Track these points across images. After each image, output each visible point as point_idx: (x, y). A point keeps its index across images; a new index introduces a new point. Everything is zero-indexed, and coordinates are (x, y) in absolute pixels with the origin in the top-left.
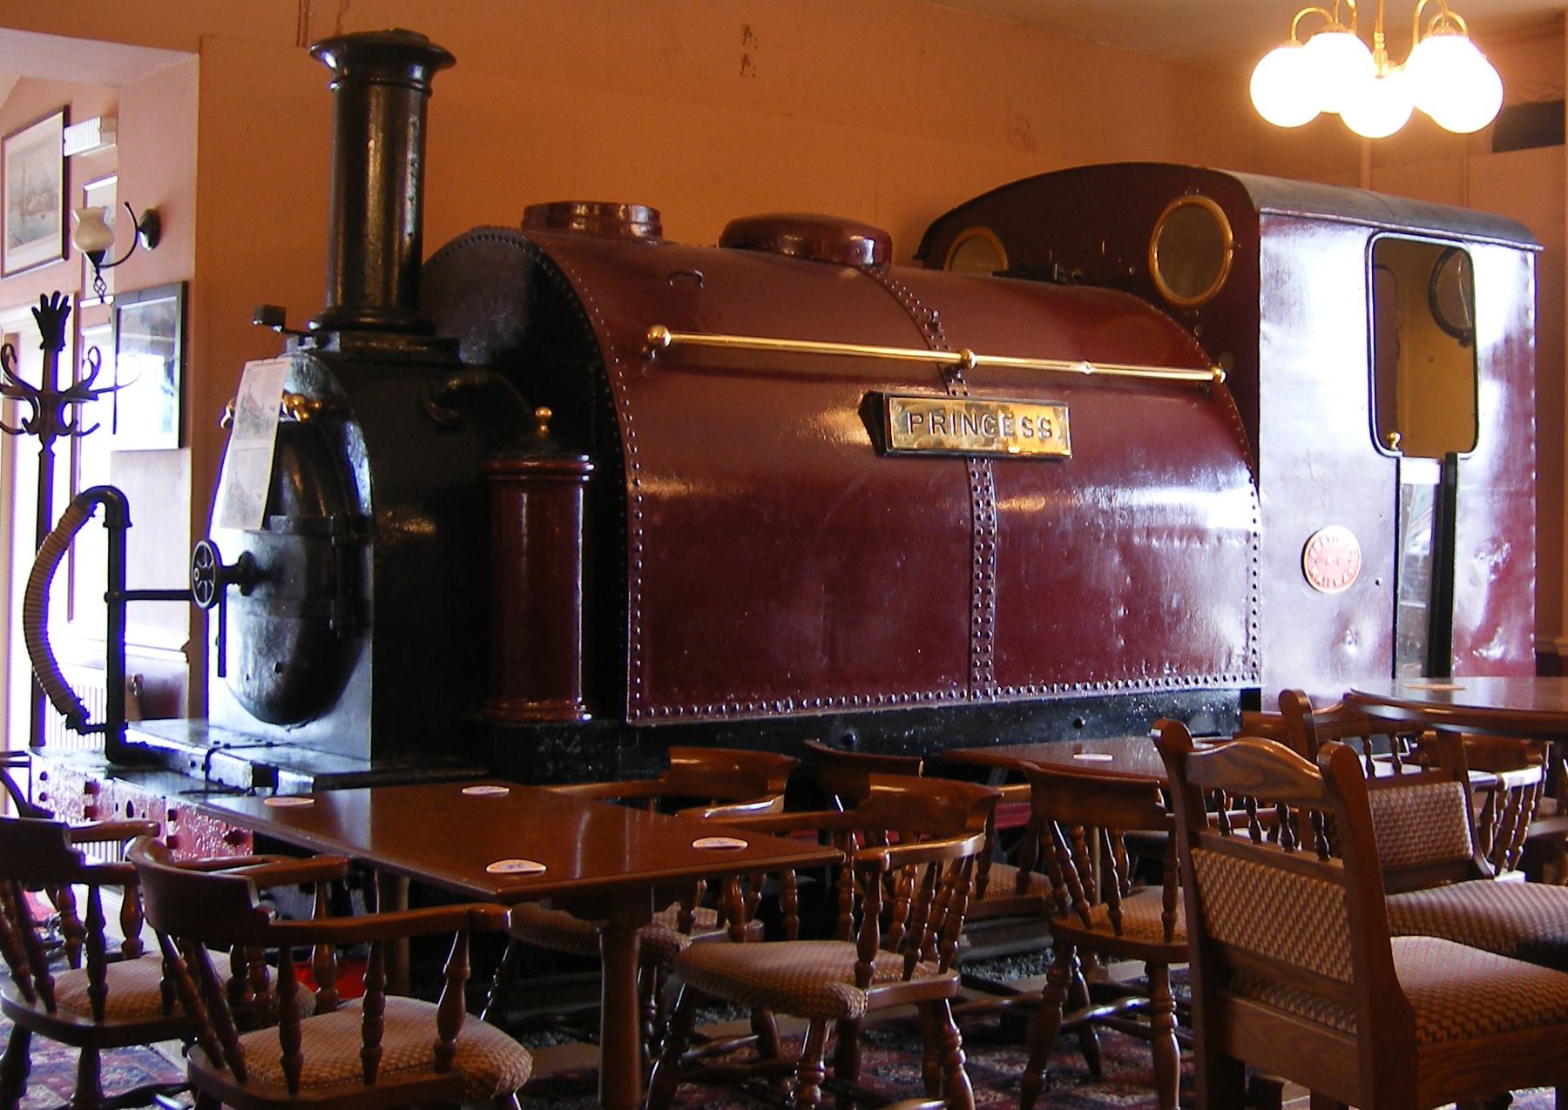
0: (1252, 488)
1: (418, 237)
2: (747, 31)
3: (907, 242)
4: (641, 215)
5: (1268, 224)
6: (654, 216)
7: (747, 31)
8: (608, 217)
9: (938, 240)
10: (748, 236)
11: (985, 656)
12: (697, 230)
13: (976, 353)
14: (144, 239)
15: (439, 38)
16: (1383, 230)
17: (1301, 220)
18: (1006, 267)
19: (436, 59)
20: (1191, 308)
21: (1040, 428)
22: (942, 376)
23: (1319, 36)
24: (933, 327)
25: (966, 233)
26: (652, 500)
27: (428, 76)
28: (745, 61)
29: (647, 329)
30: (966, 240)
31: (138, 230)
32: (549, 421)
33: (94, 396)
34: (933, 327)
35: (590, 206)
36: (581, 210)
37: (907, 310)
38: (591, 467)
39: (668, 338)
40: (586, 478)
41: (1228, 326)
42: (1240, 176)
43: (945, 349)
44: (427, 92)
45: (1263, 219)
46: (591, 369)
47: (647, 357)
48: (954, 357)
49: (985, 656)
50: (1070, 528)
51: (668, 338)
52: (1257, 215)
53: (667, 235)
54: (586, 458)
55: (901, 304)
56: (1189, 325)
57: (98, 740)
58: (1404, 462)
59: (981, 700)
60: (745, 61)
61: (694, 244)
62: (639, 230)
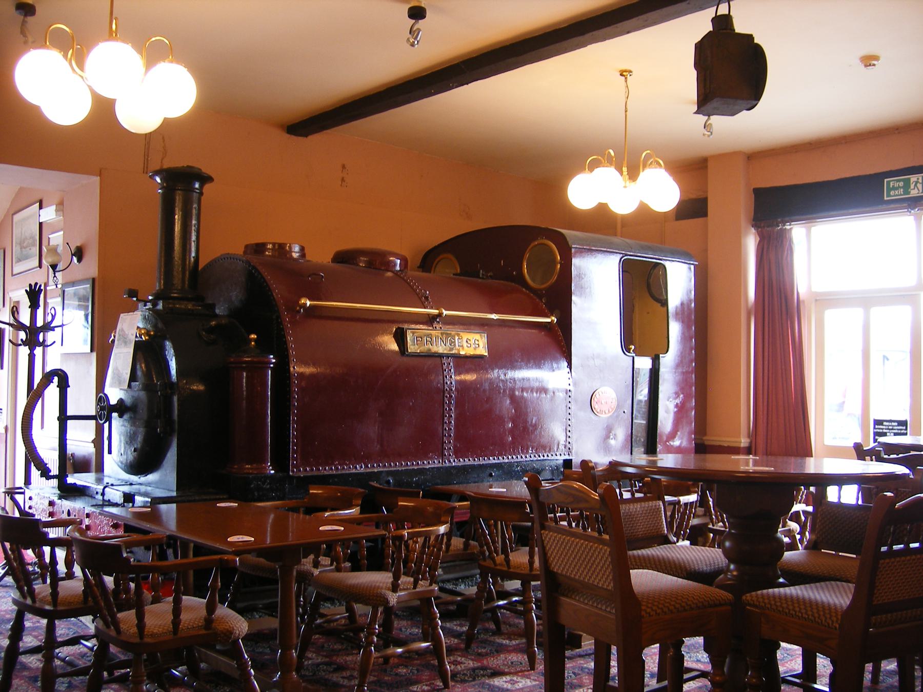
2: (344, 167)
4: (296, 248)
5: (576, 252)
6: (302, 249)
7: (344, 167)
8: (282, 249)
10: (344, 258)
11: (450, 445)
14: (75, 259)
15: (206, 170)
16: (626, 255)
17: (590, 251)
18: (459, 271)
19: (205, 179)
20: (541, 290)
21: (474, 344)
22: (430, 320)
24: (427, 298)
25: (441, 257)
27: (201, 186)
28: (343, 180)
29: (299, 299)
31: (72, 255)
33: (53, 329)
34: (427, 298)
35: (274, 244)
36: (270, 246)
37: (415, 291)
39: (308, 303)
41: (558, 298)
43: (432, 308)
44: (201, 194)
45: (573, 250)
47: (299, 312)
48: (436, 312)
49: (450, 445)
52: (570, 249)
53: (308, 258)
55: (412, 288)
57: (55, 482)
58: (636, 358)
60: (343, 180)
62: (295, 255)
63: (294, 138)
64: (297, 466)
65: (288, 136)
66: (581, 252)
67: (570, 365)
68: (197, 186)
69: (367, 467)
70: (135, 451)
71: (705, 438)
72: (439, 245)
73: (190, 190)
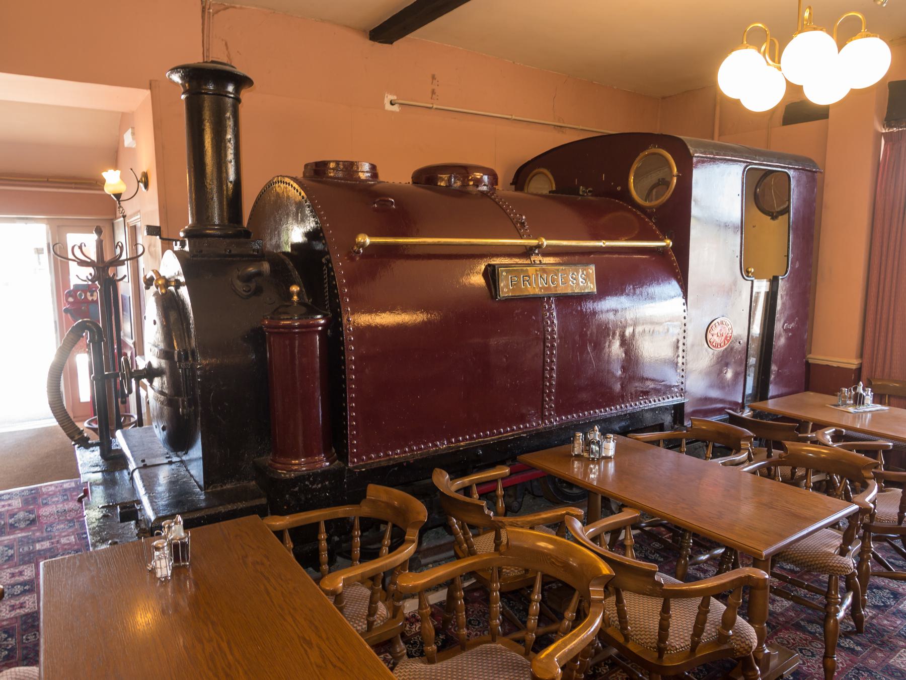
0: (684, 301)
1: (238, 183)
2: (433, 77)
3: (505, 176)
4: (366, 167)
5: (698, 162)
6: (373, 168)
7: (433, 77)
8: (350, 167)
9: (522, 175)
10: (426, 177)
11: (550, 403)
12: (398, 174)
13: (547, 239)
14: (141, 185)
15: (241, 69)
16: (751, 163)
17: (713, 160)
18: (554, 189)
19: (242, 82)
20: (651, 208)
21: (582, 280)
22: (527, 252)
23: (734, 53)
24: (523, 224)
25: (535, 172)
26: (364, 332)
27: (237, 90)
28: (433, 92)
29: (356, 236)
30: (540, 173)
31: (138, 182)
32: (299, 294)
33: (122, 263)
34: (523, 224)
35: (337, 163)
36: (332, 165)
37: (508, 215)
38: (322, 322)
39: (368, 241)
40: (320, 328)
41: (675, 217)
42: (681, 137)
43: (528, 238)
44: (237, 100)
45: (695, 160)
46: (324, 260)
47: (359, 252)
48: (534, 242)
49: (550, 403)
50: (595, 331)
51: (368, 241)
52: (691, 157)
53: (382, 177)
54: (319, 316)
55: (505, 211)
56: (650, 216)
57: (97, 451)
58: (755, 282)
59: (548, 425)
60: (433, 92)
61: (397, 182)
62: (363, 176)
63: (377, 45)
64: (358, 455)
65: (372, 42)
66: (703, 162)
67: (685, 296)
68: (230, 88)
69: (450, 442)
70: (164, 429)
71: (809, 356)
72: (532, 160)
73: (221, 94)
